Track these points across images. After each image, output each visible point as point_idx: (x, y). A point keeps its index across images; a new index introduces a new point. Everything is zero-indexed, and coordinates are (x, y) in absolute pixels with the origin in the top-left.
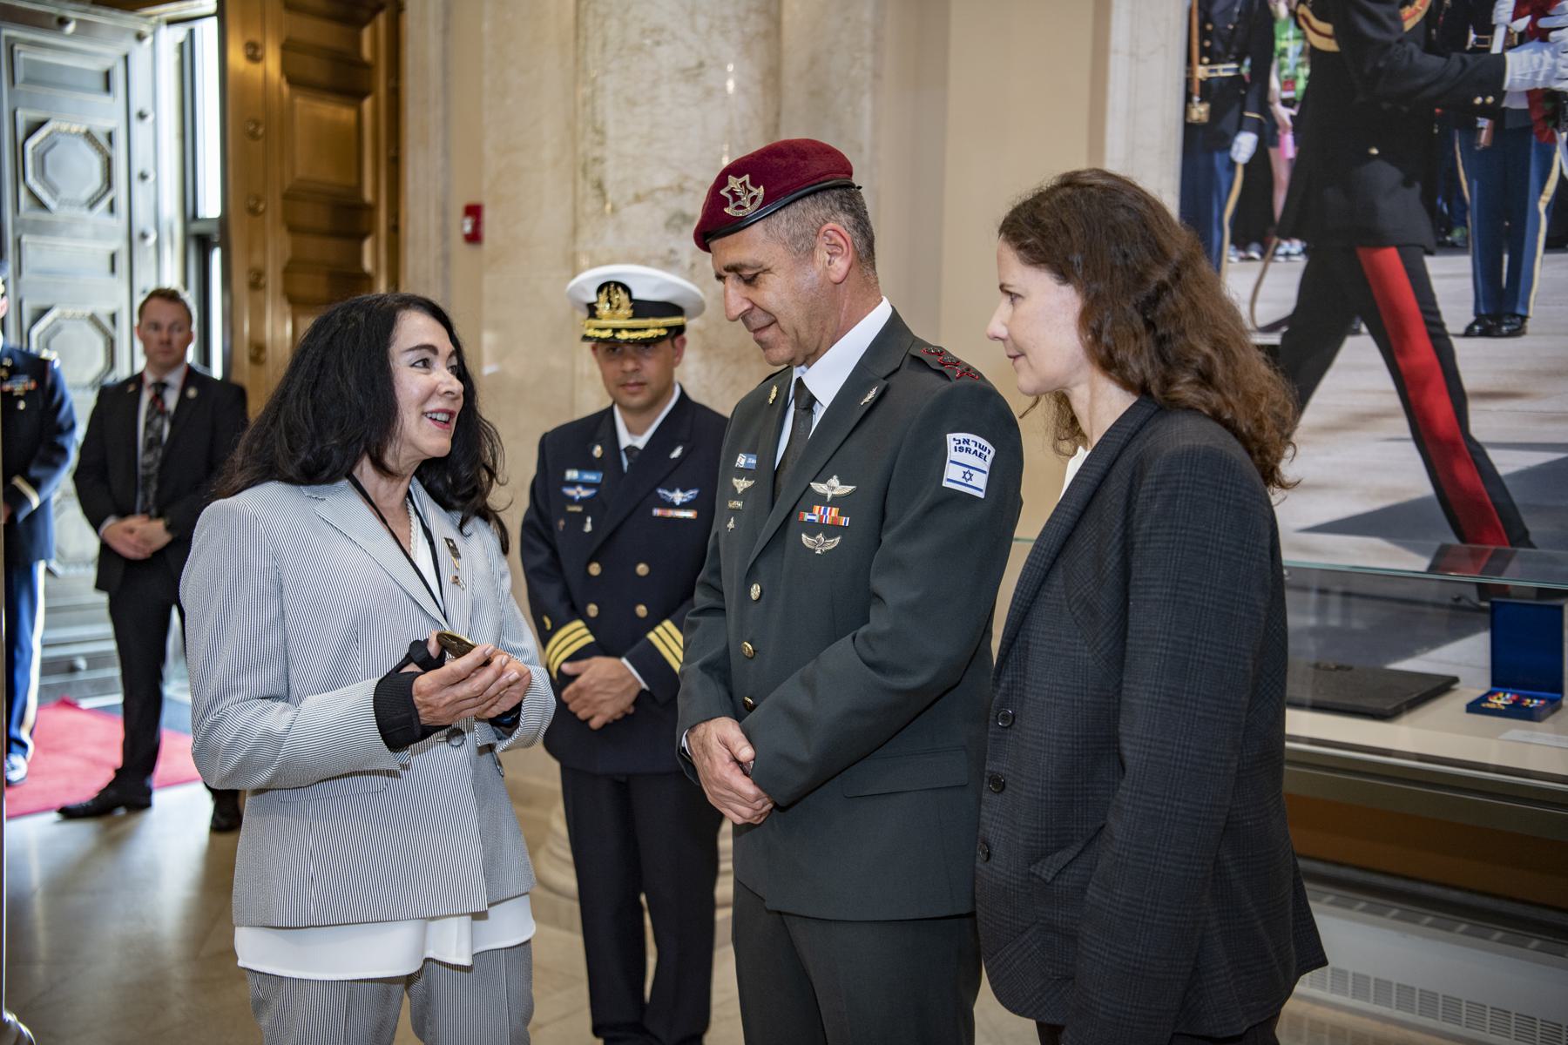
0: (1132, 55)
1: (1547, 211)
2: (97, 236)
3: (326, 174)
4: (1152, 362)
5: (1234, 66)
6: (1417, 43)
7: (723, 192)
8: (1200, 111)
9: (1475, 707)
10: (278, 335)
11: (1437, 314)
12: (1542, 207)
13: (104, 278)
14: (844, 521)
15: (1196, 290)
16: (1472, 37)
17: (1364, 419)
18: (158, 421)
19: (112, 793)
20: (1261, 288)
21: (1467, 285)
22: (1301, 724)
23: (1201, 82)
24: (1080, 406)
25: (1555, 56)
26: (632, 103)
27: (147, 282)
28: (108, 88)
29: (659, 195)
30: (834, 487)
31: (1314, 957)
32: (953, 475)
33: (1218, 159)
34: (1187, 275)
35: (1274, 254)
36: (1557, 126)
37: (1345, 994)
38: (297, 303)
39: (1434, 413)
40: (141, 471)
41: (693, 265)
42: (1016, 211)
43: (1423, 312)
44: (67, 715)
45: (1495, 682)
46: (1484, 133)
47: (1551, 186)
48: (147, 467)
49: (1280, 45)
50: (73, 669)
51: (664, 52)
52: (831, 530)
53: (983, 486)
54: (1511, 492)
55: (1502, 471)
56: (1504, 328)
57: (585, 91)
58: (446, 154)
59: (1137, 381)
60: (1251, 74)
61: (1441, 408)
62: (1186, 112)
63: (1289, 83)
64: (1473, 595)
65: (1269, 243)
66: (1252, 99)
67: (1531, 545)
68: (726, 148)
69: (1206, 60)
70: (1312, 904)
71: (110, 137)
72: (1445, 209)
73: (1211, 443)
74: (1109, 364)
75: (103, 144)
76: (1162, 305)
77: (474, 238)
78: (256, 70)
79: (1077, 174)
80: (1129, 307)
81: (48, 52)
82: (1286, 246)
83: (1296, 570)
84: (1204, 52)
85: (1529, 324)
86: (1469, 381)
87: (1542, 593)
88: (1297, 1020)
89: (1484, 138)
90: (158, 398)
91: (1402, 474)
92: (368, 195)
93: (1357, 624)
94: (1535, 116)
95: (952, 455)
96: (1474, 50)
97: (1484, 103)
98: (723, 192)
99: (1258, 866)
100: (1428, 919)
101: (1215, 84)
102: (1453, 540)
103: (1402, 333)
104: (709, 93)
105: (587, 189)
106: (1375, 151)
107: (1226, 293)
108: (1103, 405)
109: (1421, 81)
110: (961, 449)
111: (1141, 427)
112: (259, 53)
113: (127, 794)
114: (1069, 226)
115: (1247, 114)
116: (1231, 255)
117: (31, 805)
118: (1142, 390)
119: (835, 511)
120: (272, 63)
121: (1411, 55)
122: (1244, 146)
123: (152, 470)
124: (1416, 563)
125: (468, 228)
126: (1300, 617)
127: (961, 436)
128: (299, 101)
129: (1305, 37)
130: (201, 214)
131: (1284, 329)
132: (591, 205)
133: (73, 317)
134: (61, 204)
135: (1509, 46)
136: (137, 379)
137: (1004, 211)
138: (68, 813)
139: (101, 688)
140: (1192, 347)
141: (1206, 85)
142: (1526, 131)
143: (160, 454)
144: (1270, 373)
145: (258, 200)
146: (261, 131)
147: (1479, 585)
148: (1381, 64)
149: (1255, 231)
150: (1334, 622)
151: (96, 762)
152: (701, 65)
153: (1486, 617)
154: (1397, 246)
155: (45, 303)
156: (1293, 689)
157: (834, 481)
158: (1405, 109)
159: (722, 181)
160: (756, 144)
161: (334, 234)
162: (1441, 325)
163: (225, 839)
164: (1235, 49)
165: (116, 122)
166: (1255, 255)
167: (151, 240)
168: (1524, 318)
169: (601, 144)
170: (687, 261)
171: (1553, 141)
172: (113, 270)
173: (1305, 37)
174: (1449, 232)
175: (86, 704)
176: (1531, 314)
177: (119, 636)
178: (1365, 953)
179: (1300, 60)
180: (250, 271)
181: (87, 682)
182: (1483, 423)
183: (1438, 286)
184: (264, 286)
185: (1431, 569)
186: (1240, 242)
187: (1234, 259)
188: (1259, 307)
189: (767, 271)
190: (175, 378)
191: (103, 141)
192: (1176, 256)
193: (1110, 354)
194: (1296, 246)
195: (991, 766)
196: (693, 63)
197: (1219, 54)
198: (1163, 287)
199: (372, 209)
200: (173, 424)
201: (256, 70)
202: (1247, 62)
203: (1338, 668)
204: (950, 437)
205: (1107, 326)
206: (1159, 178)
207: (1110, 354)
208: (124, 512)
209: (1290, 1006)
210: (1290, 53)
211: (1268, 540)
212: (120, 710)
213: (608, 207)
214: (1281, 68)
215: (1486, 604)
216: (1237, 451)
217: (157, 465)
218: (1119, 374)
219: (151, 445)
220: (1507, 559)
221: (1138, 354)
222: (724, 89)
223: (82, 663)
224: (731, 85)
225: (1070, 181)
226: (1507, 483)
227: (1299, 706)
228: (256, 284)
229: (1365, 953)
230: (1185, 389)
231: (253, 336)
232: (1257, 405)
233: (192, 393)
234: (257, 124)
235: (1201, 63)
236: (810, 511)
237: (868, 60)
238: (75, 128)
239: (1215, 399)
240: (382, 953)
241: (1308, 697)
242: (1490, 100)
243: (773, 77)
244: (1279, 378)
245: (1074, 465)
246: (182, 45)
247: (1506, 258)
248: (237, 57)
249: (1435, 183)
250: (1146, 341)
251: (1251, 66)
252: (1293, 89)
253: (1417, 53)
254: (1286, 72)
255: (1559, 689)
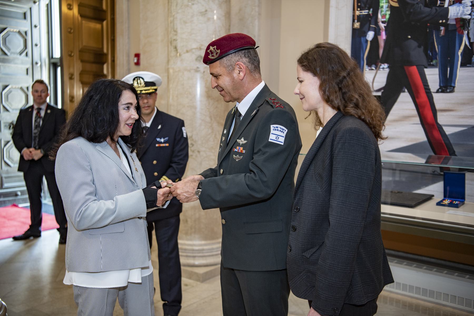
0: (337, 8)
1: (461, 55)
2: (22, 63)
3: (92, 44)
4: (341, 100)
5: (367, 11)
6: (422, 4)
7: (208, 51)
8: (357, 25)
9: (439, 204)
10: (78, 93)
11: (428, 86)
12: (459, 54)
13: (25, 76)
14: (244, 152)
15: (354, 78)
16: (439, 2)
17: (406, 118)
18: (39, 120)
19: (29, 232)
20: (376, 78)
21: (437, 77)
22: (386, 209)
23: (358, 16)
24: (320, 115)
25: (464, 8)
26: (185, 22)
27: (37, 77)
28: (25, 18)
29: (194, 50)
30: (242, 141)
31: (390, 280)
32: (272, 138)
33: (363, 39)
34: (352, 74)
35: (379, 68)
36: (464, 29)
37: (400, 290)
38: (83, 83)
39: (427, 115)
40: (33, 135)
41: (204, 72)
42: (303, 55)
43: (424, 85)
44: (15, 209)
45: (445, 196)
46: (442, 31)
47: (462, 47)
48: (35, 134)
49: (381, 4)
50: (16, 195)
51: (195, 7)
52: (240, 154)
53: (283, 141)
54: (450, 139)
55: (447, 133)
56: (448, 90)
57: (172, 19)
58: (129, 38)
59: (336, 106)
60: (373, 14)
61: (429, 114)
62: (353, 25)
63: (384, 16)
64: (438, 170)
65: (378, 65)
66: (373, 21)
67: (456, 155)
68: (214, 36)
69: (359, 9)
70: (389, 263)
71: (26, 33)
72: (431, 54)
73: (356, 126)
74: (328, 100)
75: (24, 35)
76: (344, 83)
77: (138, 64)
78: (70, 12)
79: (320, 44)
80: (334, 84)
81: (6, 7)
82: (383, 66)
83: (385, 163)
84: (358, 7)
85: (456, 89)
86: (438, 106)
87: (460, 169)
88: (385, 298)
89: (442, 33)
90: (38, 113)
91: (418, 134)
92: (105, 51)
93: (404, 180)
94: (458, 26)
95: (272, 131)
96: (439, 6)
97: (442, 22)
98: (208, 51)
99: (371, 253)
100: (425, 267)
101: (361, 16)
102: (432, 154)
103: (417, 92)
104: (209, 19)
105: (172, 48)
106: (409, 37)
107: (365, 79)
108: (328, 114)
109: (424, 15)
110: (275, 130)
111: (338, 121)
112: (71, 7)
113: (34, 232)
114: (318, 60)
115: (371, 26)
116: (366, 68)
117: (4, 236)
118: (338, 109)
119: (242, 148)
120: (76, 10)
121: (421, 7)
122: (370, 35)
123: (37, 135)
124: (422, 161)
125: (136, 61)
126: (386, 177)
127: (275, 126)
128: (84, 22)
129: (388, 2)
130: (54, 57)
131: (382, 91)
132: (173, 53)
133: (15, 88)
134: (11, 53)
135: (450, 5)
136: (32, 107)
137: (299, 55)
138: (15, 239)
139: (24, 201)
140: (353, 96)
141: (359, 17)
142: (455, 30)
143: (39, 130)
144: (377, 104)
145: (72, 52)
146: (72, 31)
147: (440, 167)
148: (412, 10)
149: (374, 61)
150: (397, 179)
151: (24, 223)
152: (206, 11)
153: (442, 177)
154: (416, 66)
155: (7, 84)
156: (383, 199)
157: (243, 139)
158: (419, 24)
159: (208, 48)
160: (223, 34)
161: (94, 63)
162: (429, 89)
163: (62, 246)
164: (368, 6)
165: (28, 28)
166: (374, 68)
167: (39, 64)
168: (454, 87)
169: (176, 35)
170: (202, 71)
171: (463, 34)
172: (27, 74)
173: (388, 2)
174: (432, 61)
175: (20, 205)
176: (456, 86)
177: (27, 185)
178: (407, 281)
179: (387, 9)
180: (69, 74)
181: (21, 199)
182: (442, 119)
183: (428, 77)
184: (74, 79)
185: (426, 163)
186: (369, 65)
187: (367, 70)
188: (375, 84)
189: (220, 75)
190: (44, 107)
191: (24, 34)
192: (349, 68)
193: (328, 97)
194: (386, 66)
195: (293, 223)
196: (204, 10)
197: (363, 8)
198: (344, 77)
199: (106, 55)
200: (43, 121)
201: (70, 12)
202: (371, 10)
203: (398, 192)
204: (272, 126)
205: (327, 89)
206: (346, 46)
207: (328, 97)
208: (29, 147)
209: (383, 293)
210: (384, 7)
211: (374, 156)
212: (29, 208)
213: (178, 54)
214: (381, 12)
215: (442, 173)
216: (365, 128)
217: (38, 133)
218: (331, 104)
219: (36, 127)
220: (449, 159)
221: (336, 98)
222: (213, 18)
223: (19, 193)
224: (215, 17)
225: (318, 46)
226: (449, 137)
227: (385, 203)
228: (71, 78)
229: (407, 281)
230: (351, 109)
231: (69, 94)
232: (371, 114)
233: (49, 111)
234: (71, 29)
235: (357, 10)
236: (236, 148)
237: (257, 9)
238: (15, 30)
239: (359, 112)
240: (115, 280)
241: (389, 201)
242: (444, 21)
243: (228, 15)
244: (380, 105)
245: (318, 132)
246: (48, 5)
247: (449, 69)
248: (65, 8)
249: (427, 46)
250: (339, 94)
251: (373, 11)
252: (385, 18)
253: (422, 7)
254: (383, 13)
255: (463, 198)
